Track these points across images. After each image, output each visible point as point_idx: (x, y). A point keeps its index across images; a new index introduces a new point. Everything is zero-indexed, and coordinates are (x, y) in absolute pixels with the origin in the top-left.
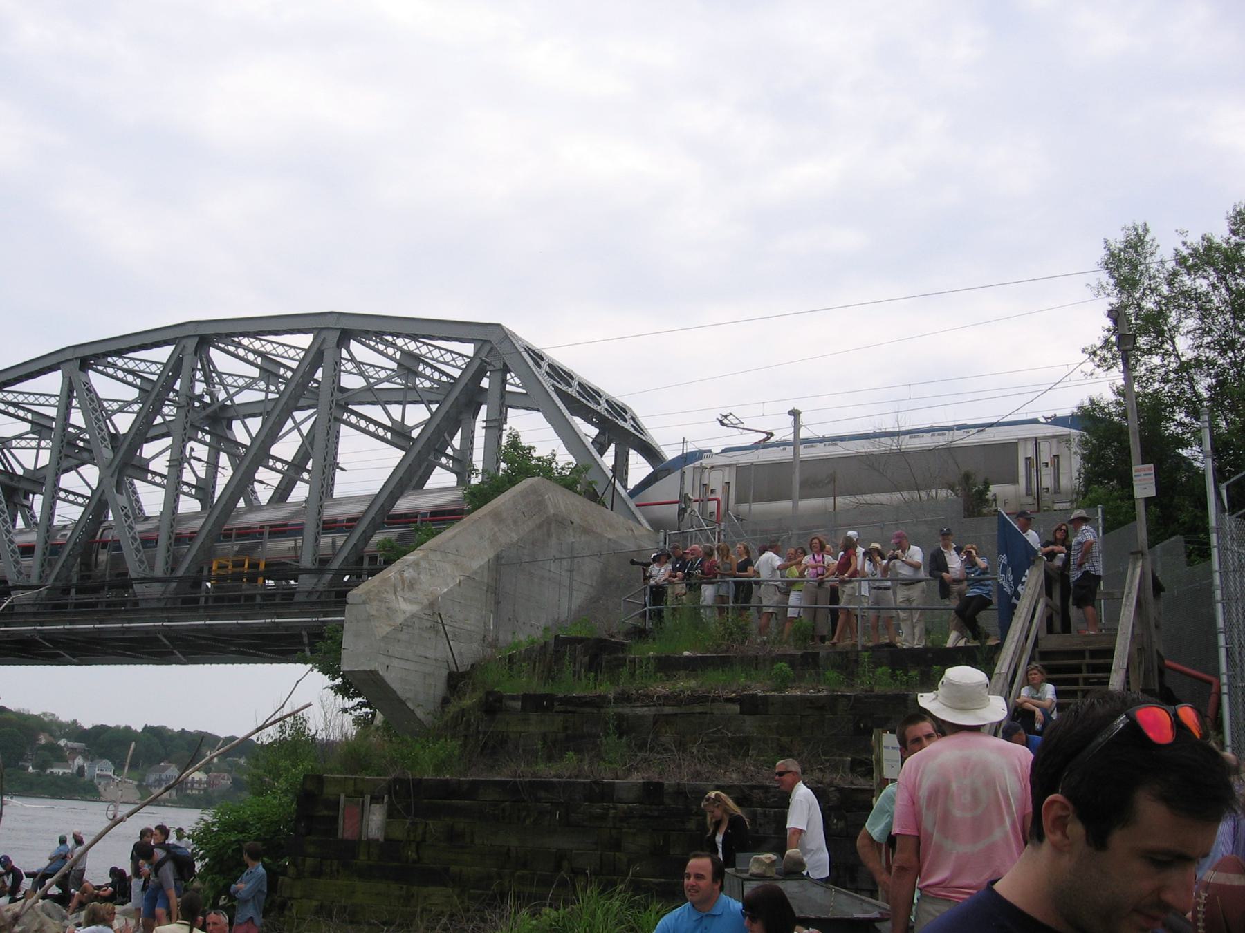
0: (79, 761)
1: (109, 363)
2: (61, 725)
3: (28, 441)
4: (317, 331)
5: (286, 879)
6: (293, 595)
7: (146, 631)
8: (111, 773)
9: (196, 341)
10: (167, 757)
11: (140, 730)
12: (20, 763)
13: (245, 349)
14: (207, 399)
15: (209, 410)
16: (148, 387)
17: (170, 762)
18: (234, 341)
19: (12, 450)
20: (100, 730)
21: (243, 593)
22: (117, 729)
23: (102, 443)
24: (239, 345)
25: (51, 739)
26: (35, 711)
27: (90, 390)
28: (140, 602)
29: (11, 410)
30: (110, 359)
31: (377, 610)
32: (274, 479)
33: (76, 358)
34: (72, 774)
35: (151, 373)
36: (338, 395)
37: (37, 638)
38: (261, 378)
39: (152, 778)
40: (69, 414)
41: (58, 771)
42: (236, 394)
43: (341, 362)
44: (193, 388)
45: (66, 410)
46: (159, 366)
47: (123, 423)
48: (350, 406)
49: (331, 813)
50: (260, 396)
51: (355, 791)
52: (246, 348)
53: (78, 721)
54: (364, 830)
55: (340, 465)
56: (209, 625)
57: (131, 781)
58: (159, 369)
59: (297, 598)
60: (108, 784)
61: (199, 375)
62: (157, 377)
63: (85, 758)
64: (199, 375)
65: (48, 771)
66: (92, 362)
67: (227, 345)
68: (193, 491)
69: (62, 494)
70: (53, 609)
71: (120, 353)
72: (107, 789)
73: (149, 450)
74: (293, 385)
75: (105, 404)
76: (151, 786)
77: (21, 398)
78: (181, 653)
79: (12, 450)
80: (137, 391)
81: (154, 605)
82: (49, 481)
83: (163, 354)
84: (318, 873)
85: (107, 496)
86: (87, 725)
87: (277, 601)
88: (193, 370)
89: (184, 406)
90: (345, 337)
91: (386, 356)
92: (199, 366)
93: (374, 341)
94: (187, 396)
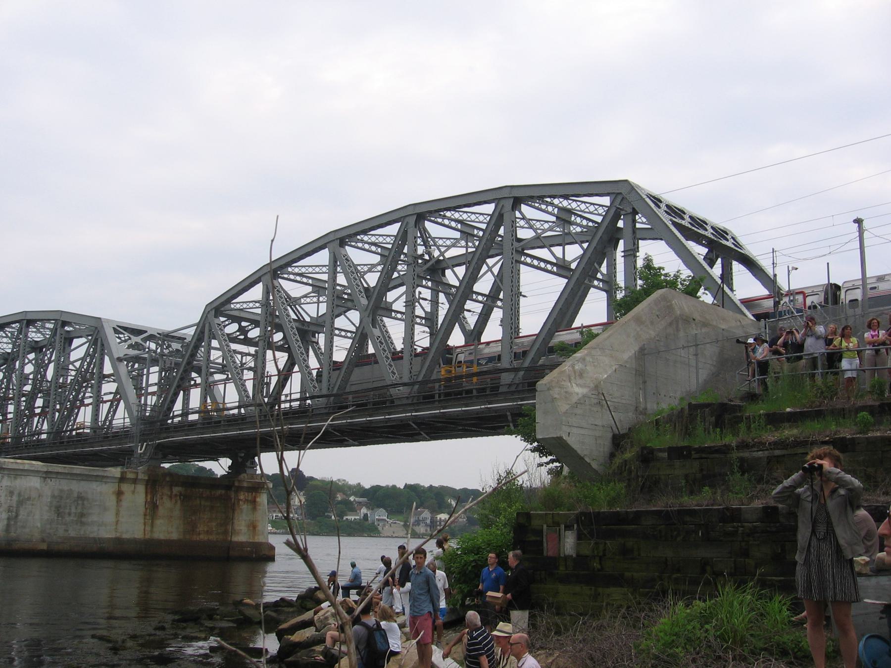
0: (364, 510)
1: (358, 239)
2: (350, 487)
3: (311, 298)
6: (498, 387)
8: (385, 518)
12: (326, 514)
13: (449, 220)
14: (427, 257)
17: (424, 508)
18: (441, 215)
20: (376, 489)
21: (464, 389)
24: (444, 217)
25: (345, 496)
29: (298, 278)
30: (359, 237)
32: (477, 308)
34: (360, 519)
36: (516, 244)
40: (336, 277)
41: (351, 518)
43: (516, 221)
44: (416, 250)
47: (372, 279)
49: (538, 539)
50: (462, 251)
52: (450, 219)
53: (361, 484)
54: (562, 550)
55: (522, 294)
57: (399, 522)
59: (501, 390)
60: (384, 525)
61: (419, 241)
62: (391, 245)
63: (368, 508)
64: (419, 241)
65: (345, 518)
67: (436, 218)
68: (423, 321)
69: (337, 332)
71: (365, 232)
72: (384, 528)
75: (359, 268)
77: (303, 270)
78: (425, 433)
81: (405, 402)
82: (328, 324)
83: (394, 229)
86: (367, 486)
88: (415, 238)
89: (411, 264)
90: (517, 202)
93: (537, 203)
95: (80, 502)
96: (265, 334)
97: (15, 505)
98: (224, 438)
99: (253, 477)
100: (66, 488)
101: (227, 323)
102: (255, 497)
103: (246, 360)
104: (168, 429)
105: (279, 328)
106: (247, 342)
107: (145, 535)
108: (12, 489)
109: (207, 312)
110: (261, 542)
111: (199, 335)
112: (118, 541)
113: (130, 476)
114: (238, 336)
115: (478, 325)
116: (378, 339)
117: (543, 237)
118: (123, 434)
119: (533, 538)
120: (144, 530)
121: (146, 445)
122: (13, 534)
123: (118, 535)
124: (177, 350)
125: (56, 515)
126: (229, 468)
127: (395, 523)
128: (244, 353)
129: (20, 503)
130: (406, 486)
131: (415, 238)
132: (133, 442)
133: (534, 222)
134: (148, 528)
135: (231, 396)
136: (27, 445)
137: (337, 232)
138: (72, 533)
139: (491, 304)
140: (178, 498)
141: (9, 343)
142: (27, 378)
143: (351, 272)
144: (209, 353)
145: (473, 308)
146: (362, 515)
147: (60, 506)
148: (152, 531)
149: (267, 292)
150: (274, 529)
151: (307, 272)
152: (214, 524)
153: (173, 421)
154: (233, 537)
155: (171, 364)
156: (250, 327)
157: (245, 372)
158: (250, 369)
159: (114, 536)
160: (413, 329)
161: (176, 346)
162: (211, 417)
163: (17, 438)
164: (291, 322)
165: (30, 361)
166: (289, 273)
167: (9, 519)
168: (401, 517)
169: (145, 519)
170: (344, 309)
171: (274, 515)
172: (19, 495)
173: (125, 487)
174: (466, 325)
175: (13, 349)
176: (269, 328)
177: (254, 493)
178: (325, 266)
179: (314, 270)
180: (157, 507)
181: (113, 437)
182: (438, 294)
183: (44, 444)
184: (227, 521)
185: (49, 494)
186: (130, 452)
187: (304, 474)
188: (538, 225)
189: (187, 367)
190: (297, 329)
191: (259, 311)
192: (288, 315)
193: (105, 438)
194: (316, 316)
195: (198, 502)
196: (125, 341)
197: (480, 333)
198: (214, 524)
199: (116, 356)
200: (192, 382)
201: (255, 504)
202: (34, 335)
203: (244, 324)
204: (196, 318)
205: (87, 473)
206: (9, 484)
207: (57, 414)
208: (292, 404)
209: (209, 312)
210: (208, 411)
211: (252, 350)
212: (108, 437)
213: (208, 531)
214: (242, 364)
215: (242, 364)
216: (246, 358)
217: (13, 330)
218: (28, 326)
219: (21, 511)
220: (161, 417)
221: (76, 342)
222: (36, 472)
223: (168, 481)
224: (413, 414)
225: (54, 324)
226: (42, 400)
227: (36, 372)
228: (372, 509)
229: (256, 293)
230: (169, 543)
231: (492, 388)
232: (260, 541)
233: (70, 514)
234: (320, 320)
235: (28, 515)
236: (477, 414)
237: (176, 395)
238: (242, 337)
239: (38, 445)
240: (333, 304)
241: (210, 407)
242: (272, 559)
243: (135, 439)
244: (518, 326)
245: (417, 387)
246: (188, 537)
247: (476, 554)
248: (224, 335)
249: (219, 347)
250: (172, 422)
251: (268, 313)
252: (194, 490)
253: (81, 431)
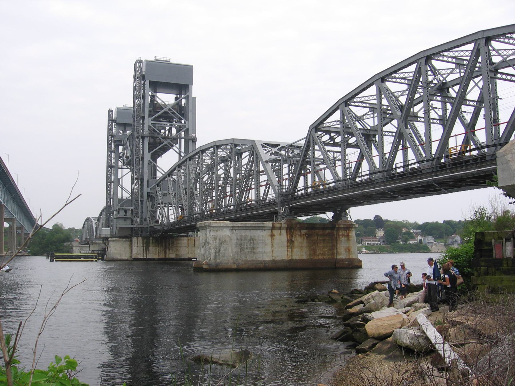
0: (419, 237)
1: (393, 77)
2: (411, 224)
3: (370, 115)
4: (475, 41)
5: (474, 276)
6: (485, 157)
7: (427, 182)
8: (433, 241)
9: (425, 59)
10: (455, 232)
11: (442, 223)
12: (397, 241)
13: (447, 57)
14: (435, 82)
15: (437, 86)
16: (410, 83)
17: (456, 234)
18: (441, 55)
19: (364, 120)
20: (426, 224)
21: (464, 160)
22: (433, 223)
23: (396, 110)
24: (444, 56)
25: (407, 230)
26: (399, 220)
27: (387, 90)
28: (422, 171)
29: (360, 104)
30: (393, 75)
31: (511, 158)
32: (471, 109)
33: (380, 78)
34: (417, 243)
35: (410, 77)
36: (490, 67)
37: (386, 191)
38: (456, 68)
39: (449, 241)
40: (381, 101)
41: (412, 242)
42: (447, 77)
43: (490, 52)
44: (427, 79)
45: (380, 99)
46: (470, 52)
47: (403, 100)
48: (499, 71)
49: (489, 248)
50: (458, 76)
51: (498, 237)
52: (447, 57)
53: (417, 222)
54: (504, 254)
55: (499, 97)
56: (452, 176)
57: (441, 243)
58: (470, 53)
59: (487, 159)
60: (432, 246)
61: (430, 73)
62: (469, 57)
63: (422, 236)
64: (430, 73)
65: (408, 243)
66: (386, 78)
67: (438, 57)
68: (438, 121)
69: (431, 121)
70: (390, 179)
71: (396, 72)
72: (432, 247)
73: (416, 109)
74: (469, 67)
75: (395, 94)
76: (450, 245)
77: (363, 99)
78: (444, 189)
79: (364, 120)
80: (407, 85)
81: (428, 171)
82: (379, 130)
83: (413, 68)
84: (487, 273)
85: (402, 131)
86: (421, 223)
87: (479, 161)
88: (426, 71)
89: (425, 87)
90: (488, 40)
91: (510, 44)
92: (429, 69)
93: (502, 39)
94: (426, 83)
95: (252, 242)
96: (344, 139)
97: (218, 245)
98: (326, 201)
99: (346, 221)
100: (243, 234)
101: (323, 135)
102: (348, 233)
103: (336, 155)
104: (295, 198)
105: (352, 135)
106: (335, 145)
107: (288, 257)
108: (216, 237)
109: (310, 130)
110: (354, 259)
111: (307, 143)
112: (274, 261)
113: (278, 225)
114: (330, 142)
115: (473, 120)
116: (409, 135)
117: (509, 60)
118: (272, 203)
119: (487, 248)
120: (288, 255)
121: (285, 208)
122: (218, 261)
123: (274, 258)
124: (298, 153)
125: (240, 249)
126: (332, 217)
127: (439, 244)
128: (335, 151)
129: (221, 244)
130: (444, 222)
131: (426, 71)
132: (277, 207)
133: (441, 71)
134: (290, 254)
135: (329, 176)
136: (224, 213)
137: (379, 75)
138: (249, 259)
139: (479, 106)
140: (305, 236)
141: (209, 159)
142: (220, 177)
143: (390, 97)
144: (314, 153)
145: (468, 111)
146: (419, 240)
147: (241, 245)
148: (292, 255)
149: (343, 115)
150: (367, 251)
151: (365, 100)
152: (326, 249)
153: (298, 193)
154: (337, 256)
155: (294, 161)
156: (336, 136)
157: (337, 162)
158: (339, 160)
159: (271, 259)
160: (430, 127)
161: (297, 151)
162: (318, 189)
163: (218, 210)
164: (358, 131)
165: (221, 168)
166: (355, 102)
167: (215, 253)
168: (442, 240)
169: (287, 248)
170: (390, 120)
171: (367, 243)
172: (220, 239)
173: (276, 232)
174: (465, 121)
175: (211, 162)
176: (6, 225)
177: (347, 231)
178: (374, 95)
179: (373, 98)
180: (294, 241)
181: (267, 205)
182: (446, 104)
183: (232, 212)
184: (334, 247)
185: (235, 238)
186: (276, 213)
187: (382, 218)
188: (505, 53)
189: (303, 162)
190: (362, 134)
191: (339, 126)
192: (356, 127)
193: (263, 206)
194: (373, 126)
195: (316, 238)
196: (269, 151)
197: (474, 125)
198: (326, 249)
199: (264, 160)
200: (308, 171)
201: (348, 237)
202: (222, 153)
203: (332, 135)
204: (305, 134)
205: (254, 226)
206: (214, 234)
207: (237, 195)
208: (363, 178)
209: (312, 130)
210: (317, 186)
211: (339, 149)
212: (264, 205)
213: (323, 254)
214: (335, 158)
215: (335, 158)
216: (336, 154)
217: (211, 152)
218: (217, 148)
219: (221, 249)
220: (291, 192)
221: (244, 155)
222: (227, 227)
223: (298, 227)
224: (434, 178)
225: (231, 146)
226: (230, 188)
227: (225, 173)
228: (424, 237)
229: (337, 116)
230: (301, 261)
231: (482, 158)
232: (353, 258)
233: (247, 248)
234: (376, 128)
235: (225, 250)
236: (474, 175)
237: (298, 178)
238: (332, 142)
239: (229, 212)
240: (381, 117)
241: (317, 184)
242: (361, 267)
243: (278, 205)
244: (498, 118)
245: (435, 161)
246: (312, 257)
247: (457, 259)
248: (321, 142)
249: (319, 149)
250: (298, 194)
251: (345, 127)
252: (313, 231)
253: (250, 203)
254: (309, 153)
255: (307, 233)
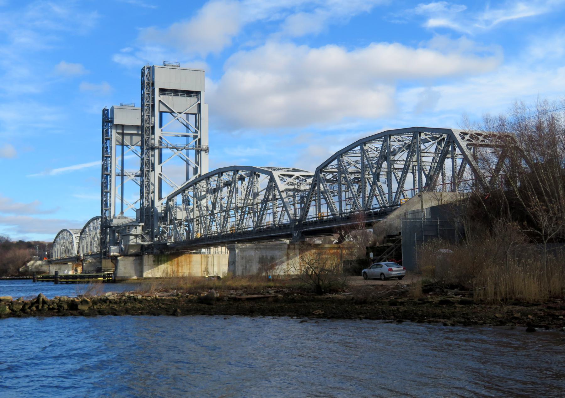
71: (350, 150)
100: (264, 254)
254: (199, 237)
255: (317, 252)
